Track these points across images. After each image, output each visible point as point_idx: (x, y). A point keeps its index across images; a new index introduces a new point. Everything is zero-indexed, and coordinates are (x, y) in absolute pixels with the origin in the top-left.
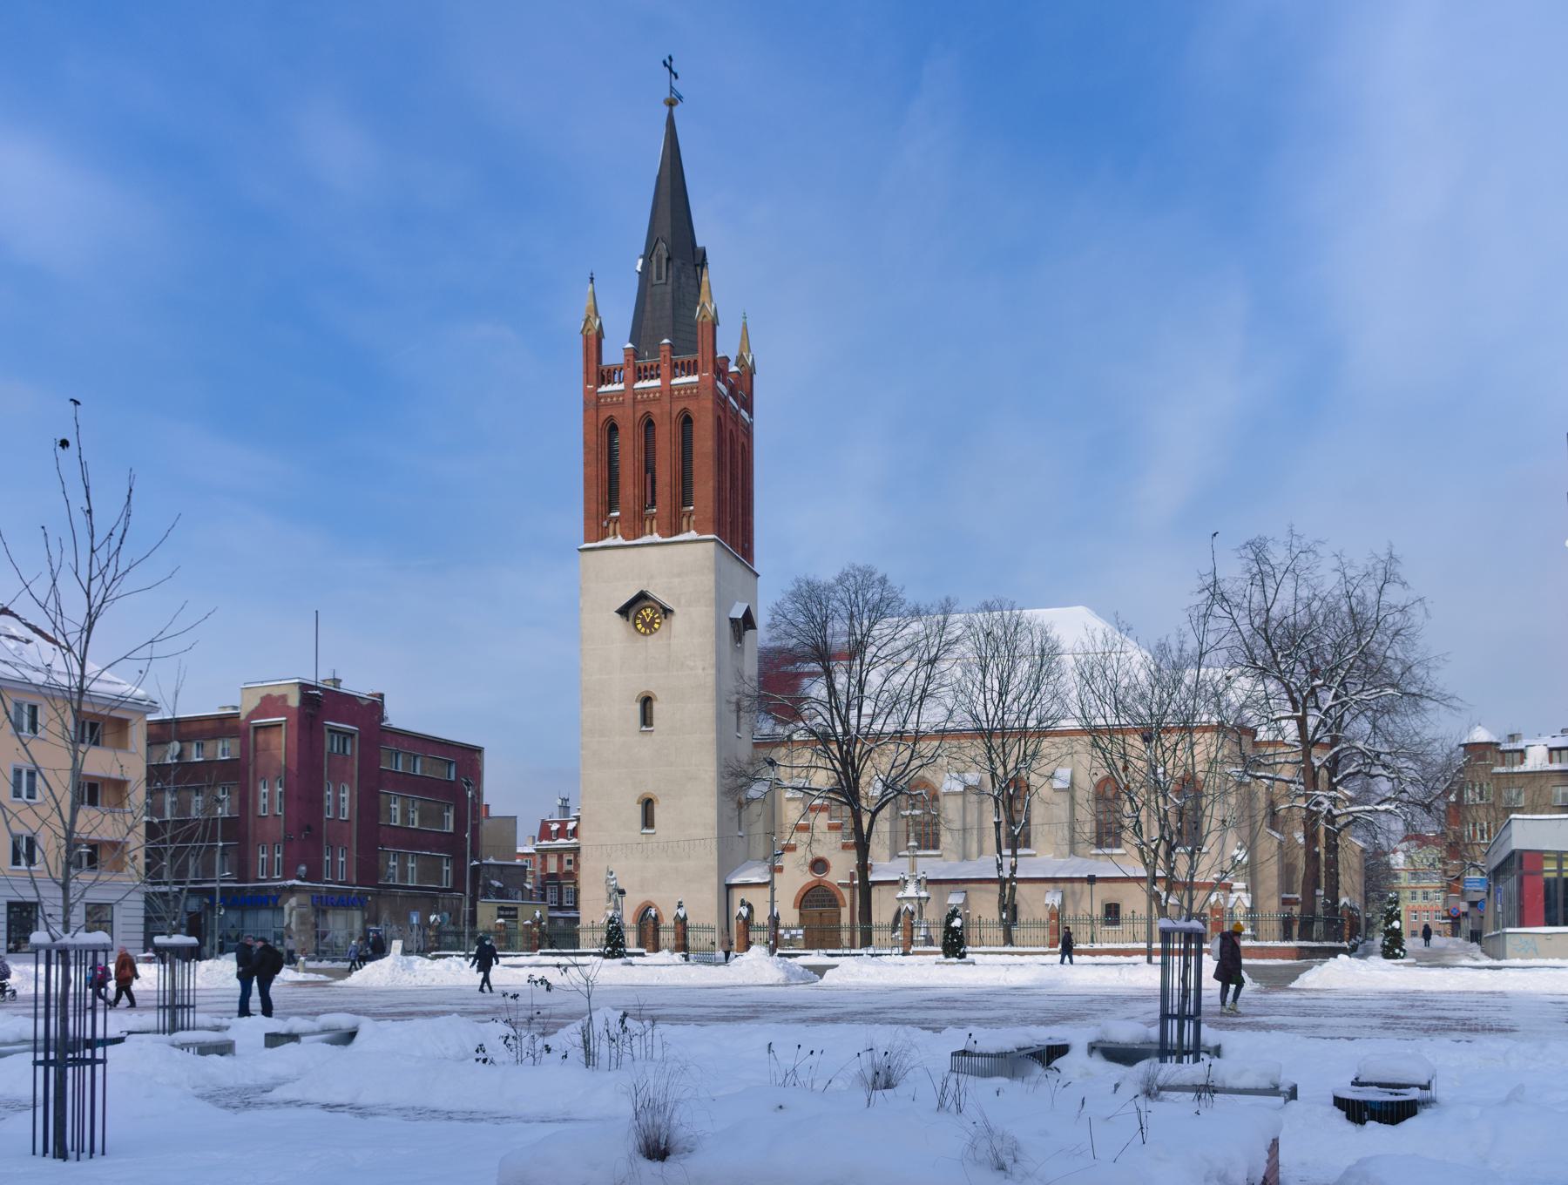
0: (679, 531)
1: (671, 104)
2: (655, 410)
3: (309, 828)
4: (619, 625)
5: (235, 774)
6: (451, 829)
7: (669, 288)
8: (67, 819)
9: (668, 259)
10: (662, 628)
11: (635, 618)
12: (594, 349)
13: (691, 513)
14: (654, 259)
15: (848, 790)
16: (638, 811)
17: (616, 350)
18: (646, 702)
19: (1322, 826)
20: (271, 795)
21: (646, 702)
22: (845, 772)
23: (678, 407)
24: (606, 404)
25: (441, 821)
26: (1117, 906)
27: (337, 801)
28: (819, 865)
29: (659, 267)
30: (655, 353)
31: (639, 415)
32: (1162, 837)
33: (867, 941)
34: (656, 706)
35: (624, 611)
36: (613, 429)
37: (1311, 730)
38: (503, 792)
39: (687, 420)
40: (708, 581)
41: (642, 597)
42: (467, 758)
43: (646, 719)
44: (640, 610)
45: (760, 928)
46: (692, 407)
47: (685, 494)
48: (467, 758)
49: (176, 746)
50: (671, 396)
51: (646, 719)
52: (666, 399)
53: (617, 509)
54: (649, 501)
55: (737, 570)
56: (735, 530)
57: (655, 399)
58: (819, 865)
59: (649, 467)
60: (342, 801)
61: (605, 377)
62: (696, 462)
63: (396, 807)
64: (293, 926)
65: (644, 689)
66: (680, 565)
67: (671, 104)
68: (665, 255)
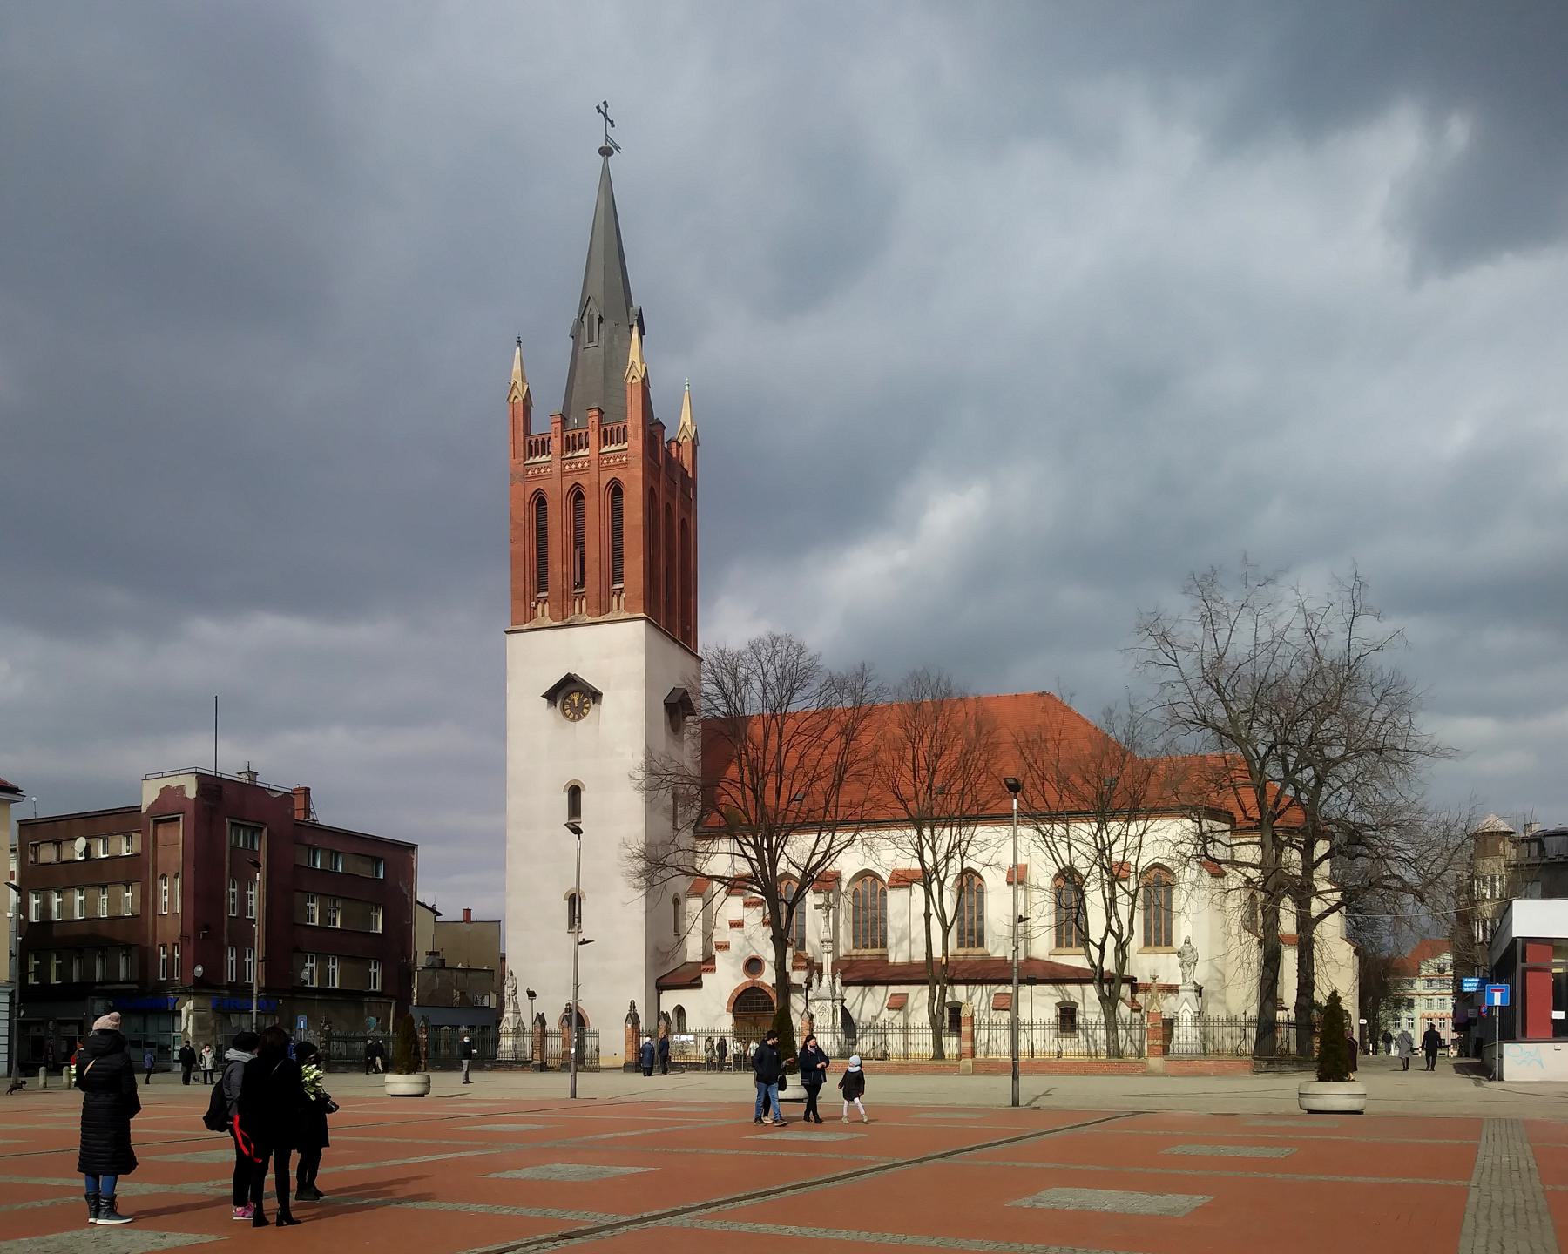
0: (608, 609)
1: (606, 152)
2: (583, 481)
3: (207, 927)
4: (548, 716)
5: (132, 871)
6: (317, 923)
7: (601, 351)
9: (600, 320)
11: (563, 704)
14: (585, 319)
17: (544, 423)
18: (575, 792)
19: (271, 1204)
20: (171, 892)
21: (575, 792)
22: (760, 859)
23: (606, 478)
25: (369, 921)
27: (243, 899)
28: (754, 965)
32: (1109, 929)
33: (1158, 944)
35: (551, 696)
36: (540, 501)
37: (1271, 800)
38: (440, 891)
39: (616, 489)
42: (399, 855)
46: (621, 475)
47: (617, 576)
48: (399, 855)
49: (81, 843)
50: (600, 464)
52: (595, 468)
53: (546, 590)
54: (578, 579)
55: (676, 653)
56: (672, 611)
58: (754, 965)
59: (579, 544)
60: (254, 899)
61: (538, 447)
63: (315, 907)
64: (190, 1031)
66: (615, 650)
67: (606, 152)
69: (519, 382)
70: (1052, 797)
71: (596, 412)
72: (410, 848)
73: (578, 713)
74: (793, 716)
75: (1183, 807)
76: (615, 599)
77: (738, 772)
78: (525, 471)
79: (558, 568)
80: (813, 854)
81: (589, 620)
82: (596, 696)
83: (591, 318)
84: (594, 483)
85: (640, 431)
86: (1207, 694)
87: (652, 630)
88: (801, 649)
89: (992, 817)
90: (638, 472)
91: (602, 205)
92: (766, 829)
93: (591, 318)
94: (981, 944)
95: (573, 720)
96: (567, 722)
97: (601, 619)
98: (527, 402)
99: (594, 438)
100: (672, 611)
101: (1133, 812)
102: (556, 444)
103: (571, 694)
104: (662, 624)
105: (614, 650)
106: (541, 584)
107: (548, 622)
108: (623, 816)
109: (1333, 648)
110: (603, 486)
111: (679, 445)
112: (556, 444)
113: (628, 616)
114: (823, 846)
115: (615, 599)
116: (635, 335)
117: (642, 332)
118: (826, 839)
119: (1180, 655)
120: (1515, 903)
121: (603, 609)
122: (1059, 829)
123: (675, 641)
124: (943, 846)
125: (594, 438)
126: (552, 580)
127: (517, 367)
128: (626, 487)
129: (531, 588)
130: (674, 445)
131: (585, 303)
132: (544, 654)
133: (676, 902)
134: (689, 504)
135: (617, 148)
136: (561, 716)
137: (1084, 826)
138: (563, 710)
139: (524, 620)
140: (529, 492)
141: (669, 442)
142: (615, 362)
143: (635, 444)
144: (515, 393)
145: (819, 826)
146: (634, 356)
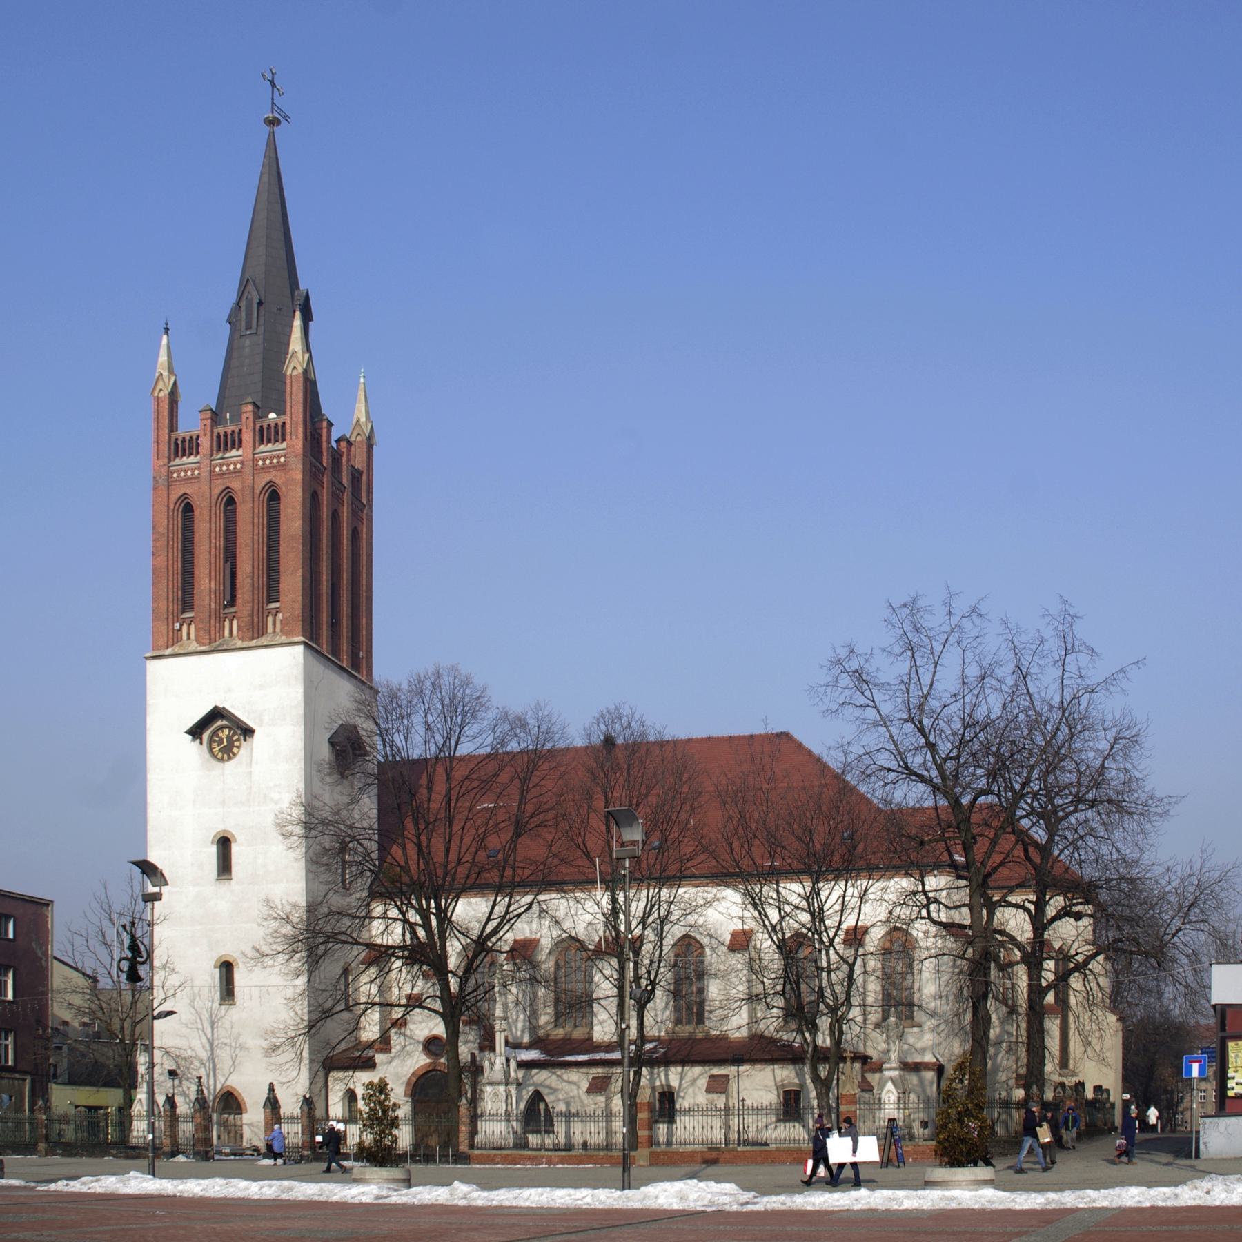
1: (272, 122)
2: (235, 485)
4: (194, 751)
8: (209, 1035)
9: (260, 303)
10: (244, 750)
11: (211, 741)
12: (166, 414)
13: (277, 611)
14: (243, 304)
15: (556, 983)
16: (212, 977)
17: (191, 423)
18: (224, 843)
21: (224, 843)
23: (262, 480)
24: (180, 480)
26: (1134, 740)
29: (249, 314)
30: (237, 418)
31: (217, 491)
34: (235, 849)
35: (196, 731)
36: (188, 509)
39: (274, 496)
40: (295, 694)
41: (216, 714)
43: (225, 866)
44: (220, 730)
45: (292, 1119)
46: (279, 478)
47: (273, 593)
51: (225, 866)
52: (248, 470)
53: (191, 609)
54: (228, 596)
57: (235, 471)
59: (230, 555)
62: (283, 547)
65: (221, 827)
68: (256, 301)
69: (165, 373)
70: (758, 851)
71: (250, 408)
72: (47, 904)
73: (227, 752)
74: (462, 759)
75: (895, 867)
76: (270, 619)
77: (413, 825)
78: (169, 473)
79: (206, 584)
80: (489, 919)
81: (239, 644)
82: (248, 732)
83: (250, 302)
84: (247, 490)
85: (300, 429)
86: (910, 737)
87: (309, 652)
88: (467, 683)
89: (693, 876)
90: (297, 475)
91: (265, 179)
92: (430, 887)
93: (250, 302)
94: (700, 1018)
95: (222, 760)
96: (220, 765)
97: (253, 643)
98: (173, 394)
99: (247, 437)
100: (338, 629)
101: (846, 870)
102: (205, 442)
103: (220, 730)
104: (325, 649)
105: (269, 679)
106: (187, 602)
107: (194, 646)
108: (279, 874)
109: (1047, 688)
110: (257, 491)
111: (350, 444)
112: (205, 442)
113: (284, 639)
114: (499, 910)
115: (270, 619)
116: (298, 322)
117: (307, 317)
118: (503, 902)
119: (878, 696)
120: (875, 1138)
121: (255, 633)
122: (768, 891)
123: (342, 668)
124: (638, 908)
125: (247, 437)
126: (204, 592)
127: (163, 358)
128: (283, 491)
129: (175, 607)
130: (344, 444)
131: (244, 284)
132: (182, 686)
133: (346, 972)
134: (361, 508)
135: (286, 117)
136: (207, 755)
137: (796, 887)
138: (211, 749)
139: (168, 644)
140: (174, 497)
141: (338, 441)
142: (276, 350)
143: (296, 441)
144: (160, 385)
145: (500, 888)
146: (296, 344)
